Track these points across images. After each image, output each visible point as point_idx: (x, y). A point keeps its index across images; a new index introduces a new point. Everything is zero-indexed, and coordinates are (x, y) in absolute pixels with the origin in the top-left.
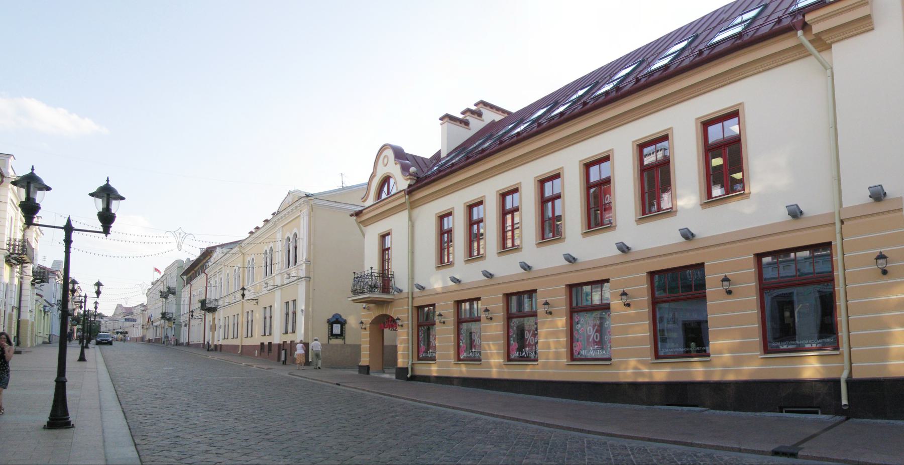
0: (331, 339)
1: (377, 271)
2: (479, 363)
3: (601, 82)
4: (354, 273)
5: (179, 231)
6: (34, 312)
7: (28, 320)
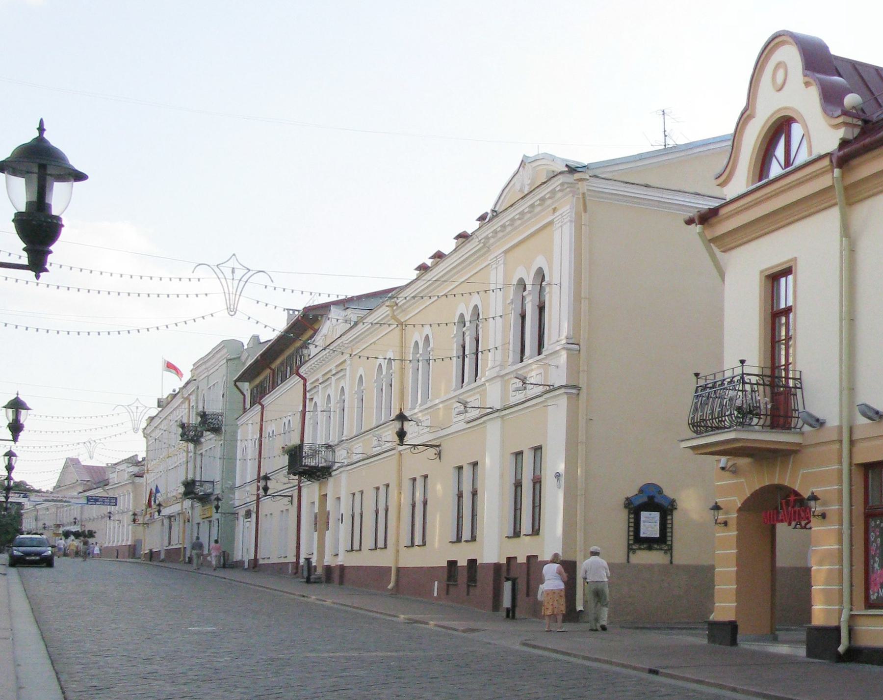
0: (634, 551)
1: (756, 371)
4: (697, 375)
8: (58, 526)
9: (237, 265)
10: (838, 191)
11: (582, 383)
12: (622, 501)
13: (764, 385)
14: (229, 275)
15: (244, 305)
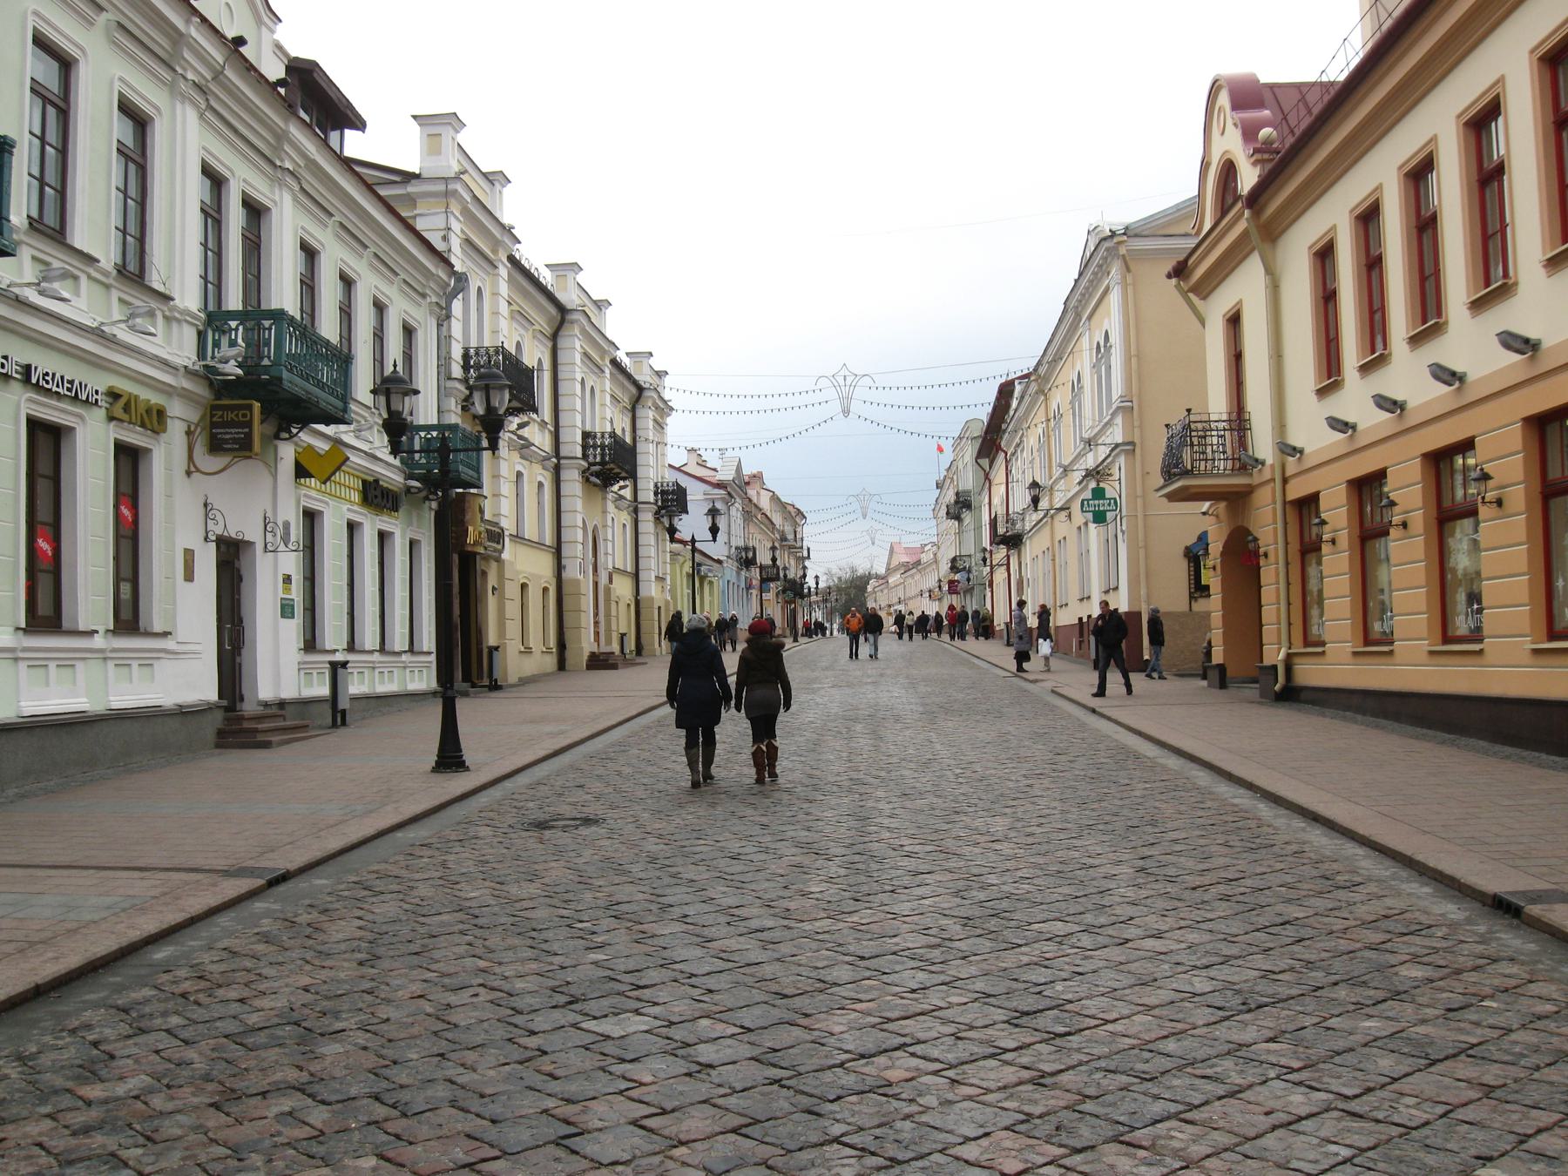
0: (1196, 599)
1: (1225, 417)
2: (1319, 650)
3: (408, 357)
4: (1167, 426)
5: (842, 373)
6: (668, 578)
7: (652, 599)
8: (890, 606)
9: (847, 373)
10: (1255, 237)
11: (1136, 441)
12: (1181, 551)
13: (1231, 430)
14: (842, 383)
15: (855, 407)
